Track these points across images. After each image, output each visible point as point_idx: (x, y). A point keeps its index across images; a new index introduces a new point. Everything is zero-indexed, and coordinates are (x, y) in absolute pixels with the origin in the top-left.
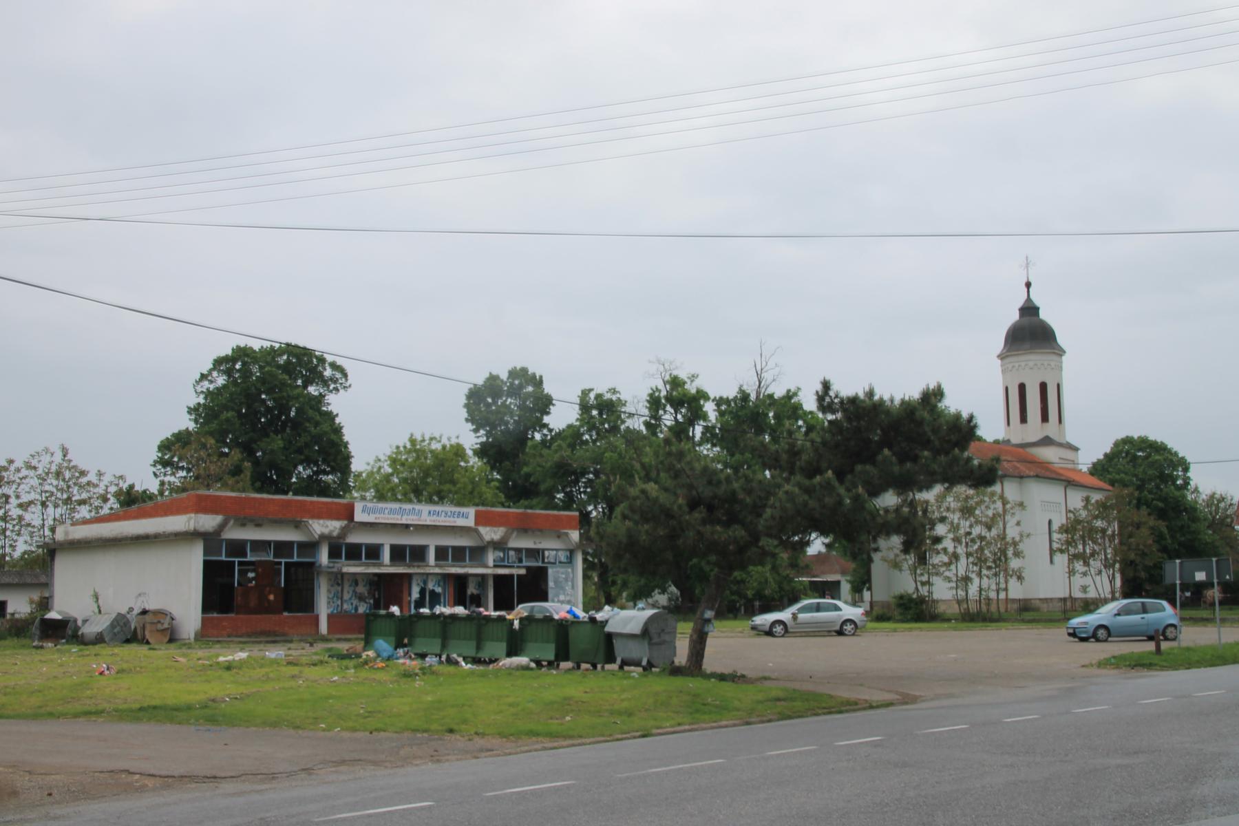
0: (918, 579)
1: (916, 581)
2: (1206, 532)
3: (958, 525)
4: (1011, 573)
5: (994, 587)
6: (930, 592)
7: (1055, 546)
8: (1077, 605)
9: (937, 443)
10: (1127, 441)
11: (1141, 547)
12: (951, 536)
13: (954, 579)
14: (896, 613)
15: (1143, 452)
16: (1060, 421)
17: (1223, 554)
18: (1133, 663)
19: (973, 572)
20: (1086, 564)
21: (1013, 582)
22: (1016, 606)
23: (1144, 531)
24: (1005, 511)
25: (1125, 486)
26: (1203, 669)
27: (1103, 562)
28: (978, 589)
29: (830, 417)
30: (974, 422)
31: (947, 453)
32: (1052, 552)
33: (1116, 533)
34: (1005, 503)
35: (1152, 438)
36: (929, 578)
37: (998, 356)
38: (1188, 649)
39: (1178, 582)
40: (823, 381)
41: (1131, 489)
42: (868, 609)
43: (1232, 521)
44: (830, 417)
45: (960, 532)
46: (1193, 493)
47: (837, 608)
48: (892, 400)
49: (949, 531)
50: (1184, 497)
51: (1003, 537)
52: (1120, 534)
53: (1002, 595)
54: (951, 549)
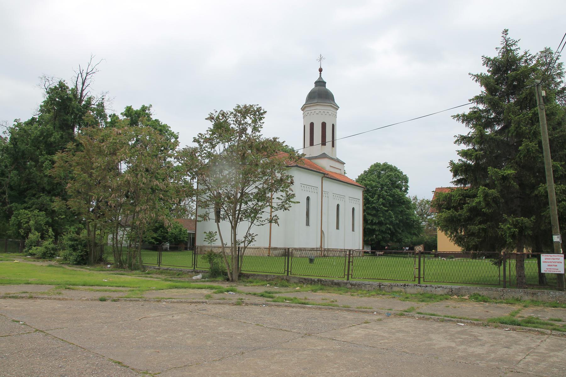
10: (377, 165)
16: (333, 146)
35: (389, 163)
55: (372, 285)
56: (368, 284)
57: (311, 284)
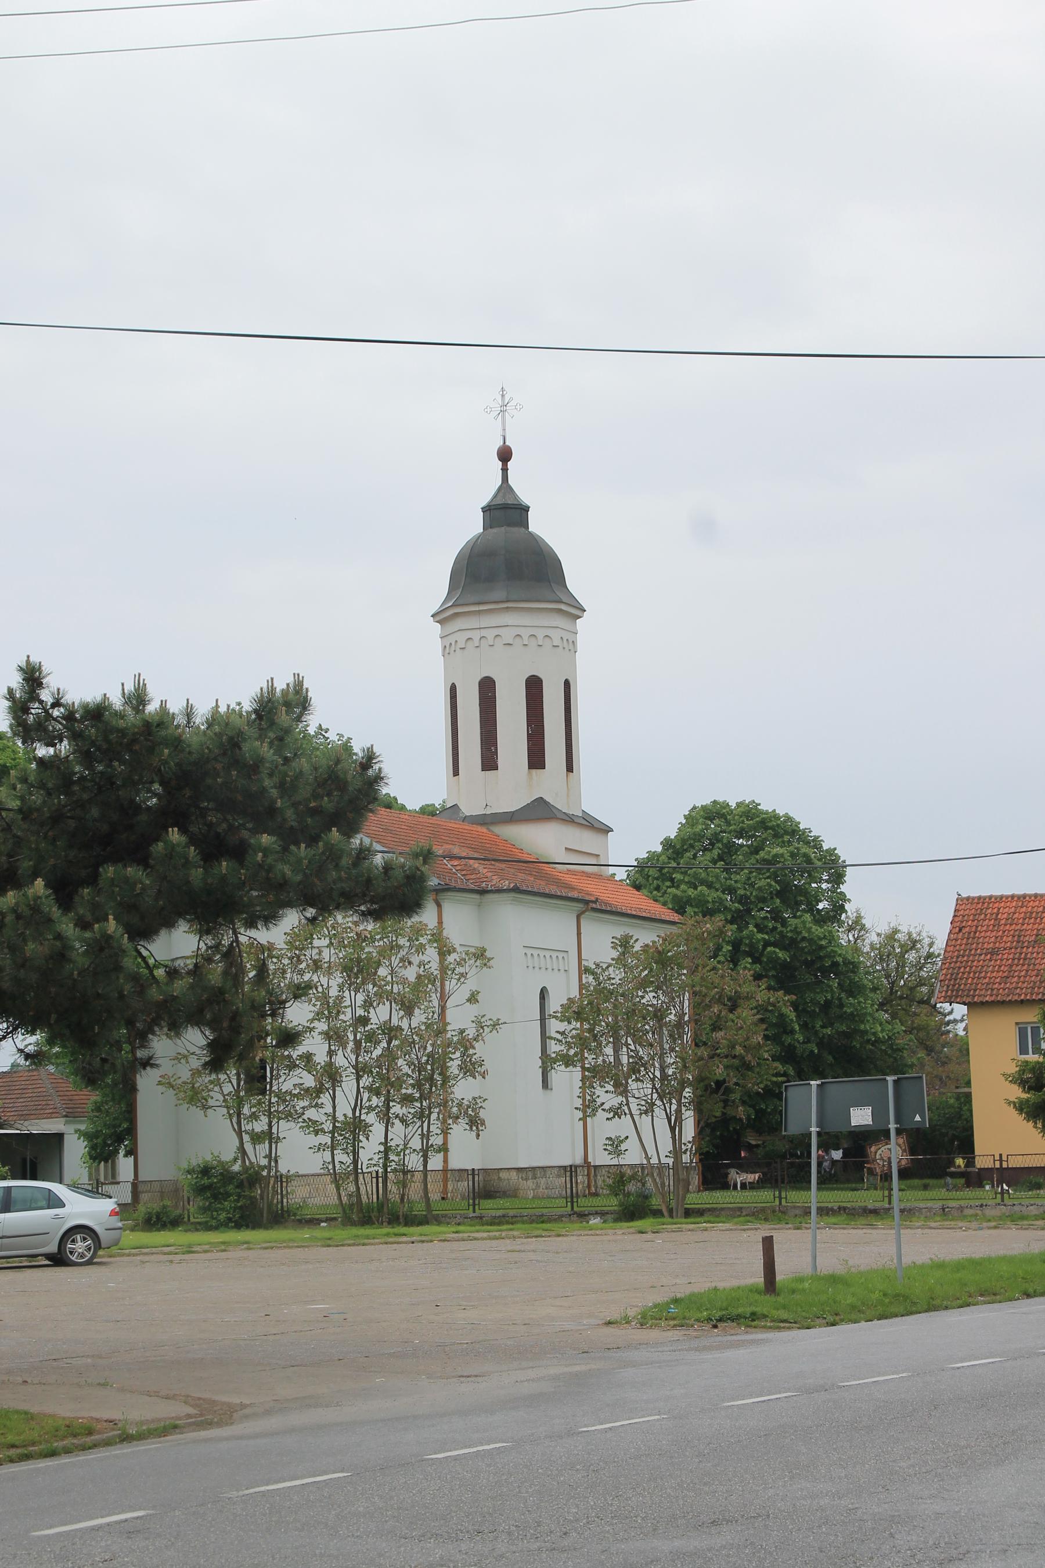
0: (246, 1126)
1: (239, 1133)
2: (877, 1015)
3: (340, 999)
4: (455, 1110)
5: (416, 1143)
6: (272, 1158)
7: (554, 1048)
8: (600, 1183)
9: (290, 814)
10: (715, 812)
11: (739, 1050)
12: (322, 1026)
13: (328, 1126)
14: (193, 1209)
15: (748, 838)
17: (912, 1066)
18: (718, 1314)
19: (370, 1109)
20: (621, 1088)
21: (459, 1131)
22: (463, 1186)
23: (746, 1015)
24: (443, 969)
25: (708, 913)
26: (863, 1324)
27: (658, 1086)
28: (382, 1148)
29: (43, 751)
30: (376, 767)
31: (313, 840)
32: (547, 1063)
33: (686, 1018)
34: (444, 951)
35: (766, 806)
36: (270, 1126)
37: (482, 508)
38: (833, 1280)
39: (814, 1129)
40: (24, 665)
41: (719, 919)
42: (128, 1199)
43: (931, 993)
44: (43, 751)
45: (342, 1017)
46: (850, 929)
47: (54, 1202)
48: (189, 714)
49: (318, 1016)
50: (832, 939)
51: (437, 1027)
52: (696, 1021)
53: (435, 1162)
54: (321, 1057)
55: (931, 1208)
56: (925, 1208)
57: (827, 1214)
